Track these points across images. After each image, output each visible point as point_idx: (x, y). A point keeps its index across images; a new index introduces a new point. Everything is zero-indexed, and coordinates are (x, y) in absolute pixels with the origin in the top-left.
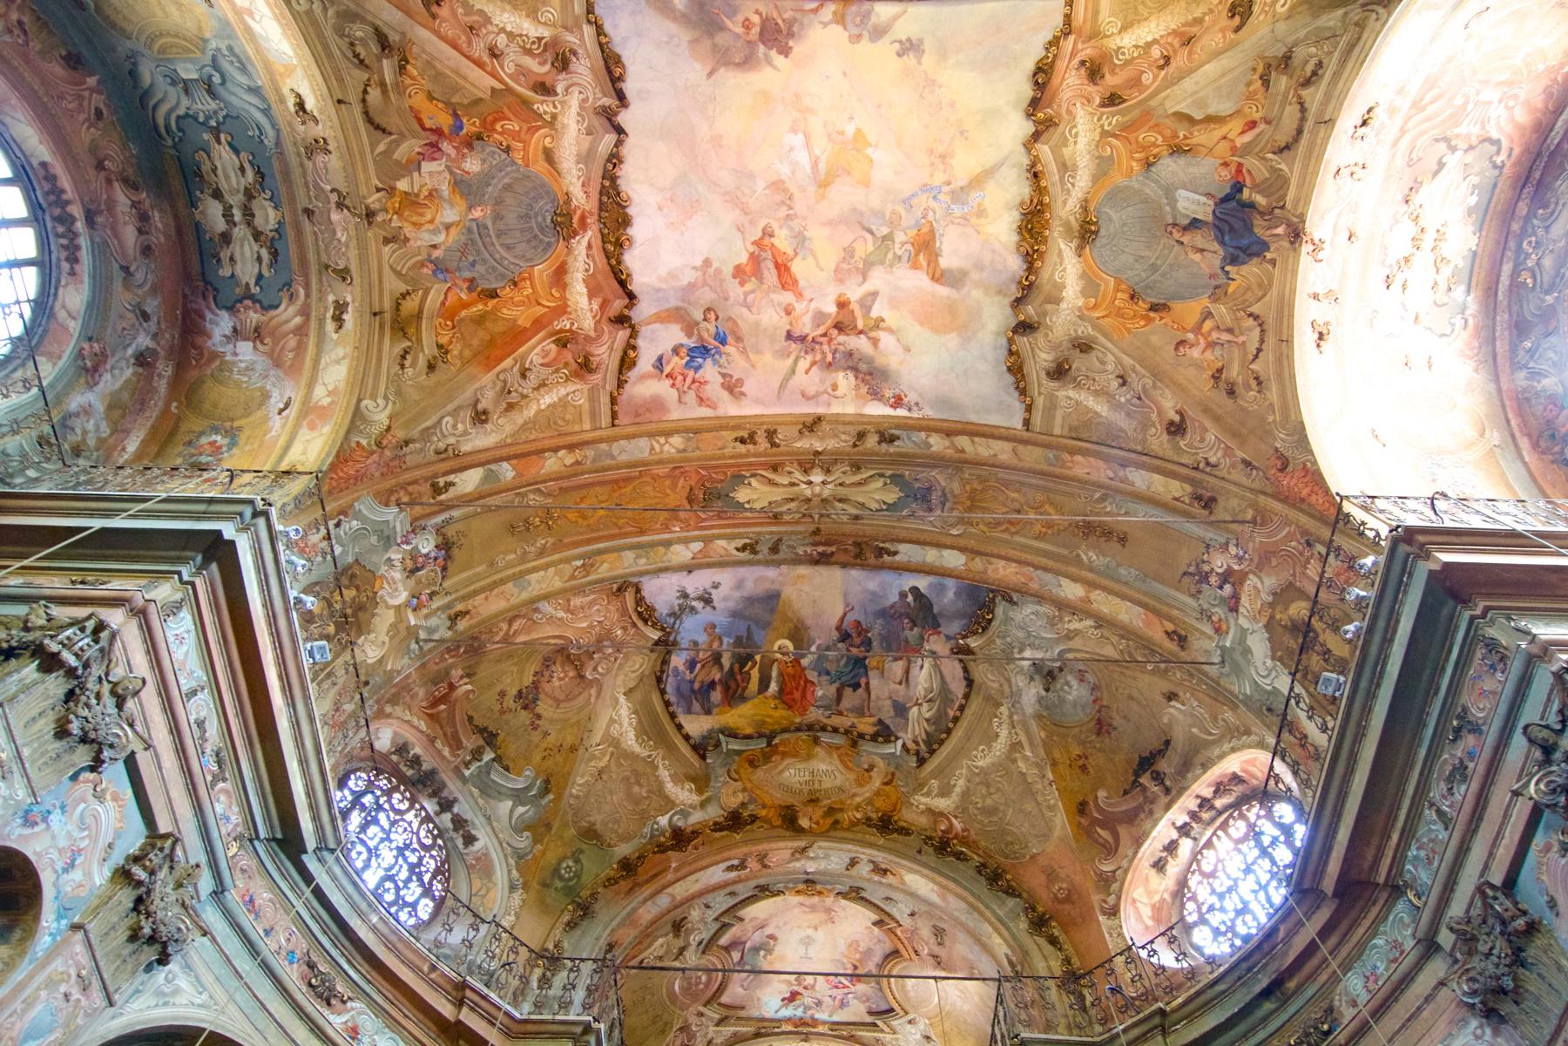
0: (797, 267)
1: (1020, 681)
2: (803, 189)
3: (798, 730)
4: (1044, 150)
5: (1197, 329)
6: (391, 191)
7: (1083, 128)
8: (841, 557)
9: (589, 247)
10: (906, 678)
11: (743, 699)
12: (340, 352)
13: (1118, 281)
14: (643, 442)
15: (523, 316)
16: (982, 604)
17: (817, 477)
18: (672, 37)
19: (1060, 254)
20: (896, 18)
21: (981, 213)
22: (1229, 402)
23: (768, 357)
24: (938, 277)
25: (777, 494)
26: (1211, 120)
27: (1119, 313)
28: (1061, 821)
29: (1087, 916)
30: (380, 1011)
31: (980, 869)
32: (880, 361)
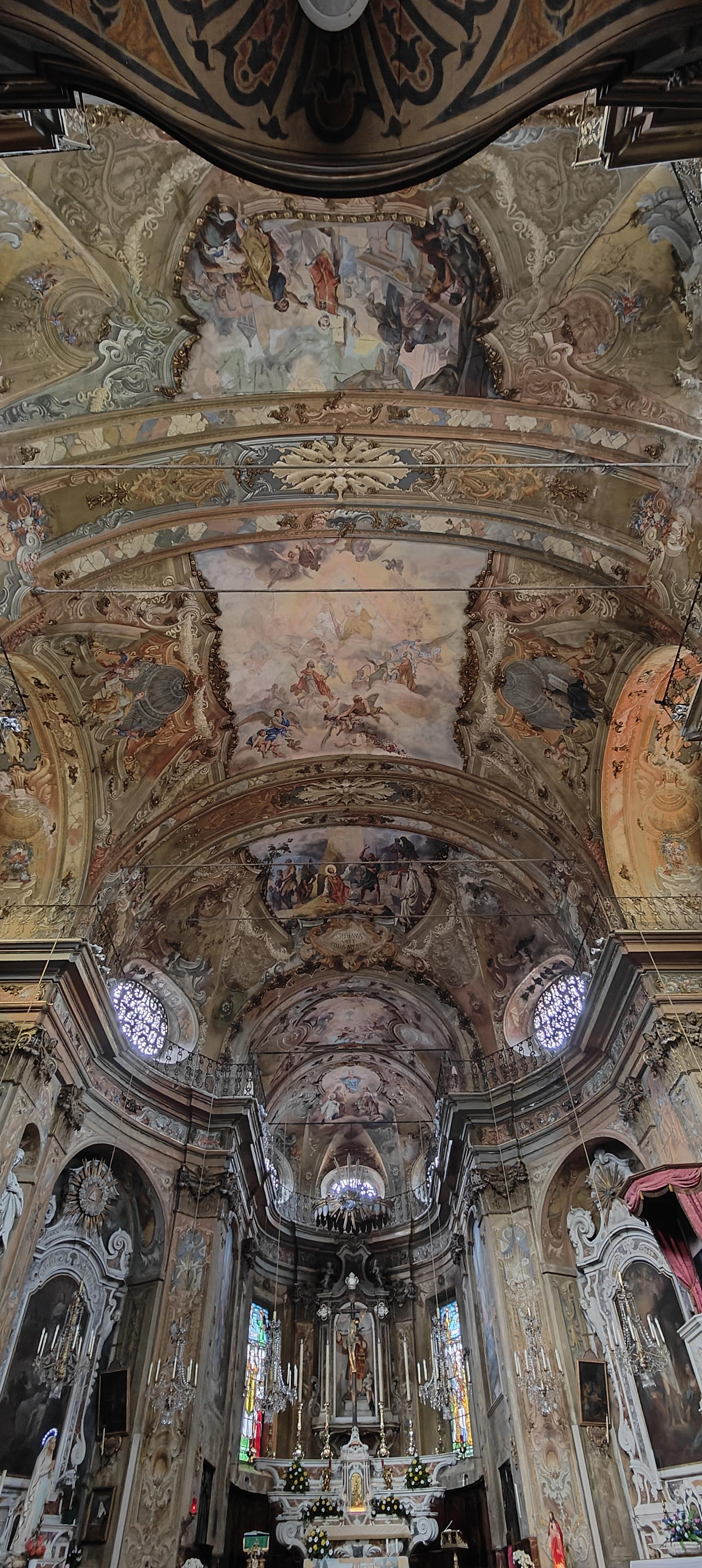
0: (329, 682)
1: (462, 892)
2: (331, 641)
3: (341, 913)
4: (475, 634)
5: (557, 745)
6: (91, 701)
7: (498, 631)
8: (362, 822)
9: (205, 694)
10: (399, 884)
11: (310, 899)
12: (77, 795)
13: (516, 710)
14: (245, 782)
15: (170, 741)
16: (441, 848)
17: (340, 482)
18: (244, 570)
19: (484, 689)
20: (385, 548)
21: (439, 660)
22: (569, 790)
23: (314, 729)
24: (415, 689)
25: (323, 794)
26: (566, 646)
27: (516, 726)
28: (480, 969)
29: (487, 1021)
30: (155, 1108)
31: (437, 990)
32: (381, 729)
